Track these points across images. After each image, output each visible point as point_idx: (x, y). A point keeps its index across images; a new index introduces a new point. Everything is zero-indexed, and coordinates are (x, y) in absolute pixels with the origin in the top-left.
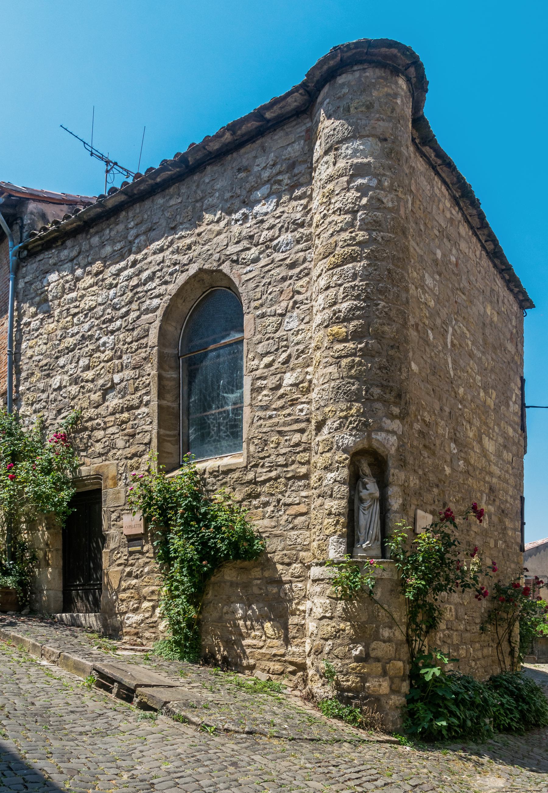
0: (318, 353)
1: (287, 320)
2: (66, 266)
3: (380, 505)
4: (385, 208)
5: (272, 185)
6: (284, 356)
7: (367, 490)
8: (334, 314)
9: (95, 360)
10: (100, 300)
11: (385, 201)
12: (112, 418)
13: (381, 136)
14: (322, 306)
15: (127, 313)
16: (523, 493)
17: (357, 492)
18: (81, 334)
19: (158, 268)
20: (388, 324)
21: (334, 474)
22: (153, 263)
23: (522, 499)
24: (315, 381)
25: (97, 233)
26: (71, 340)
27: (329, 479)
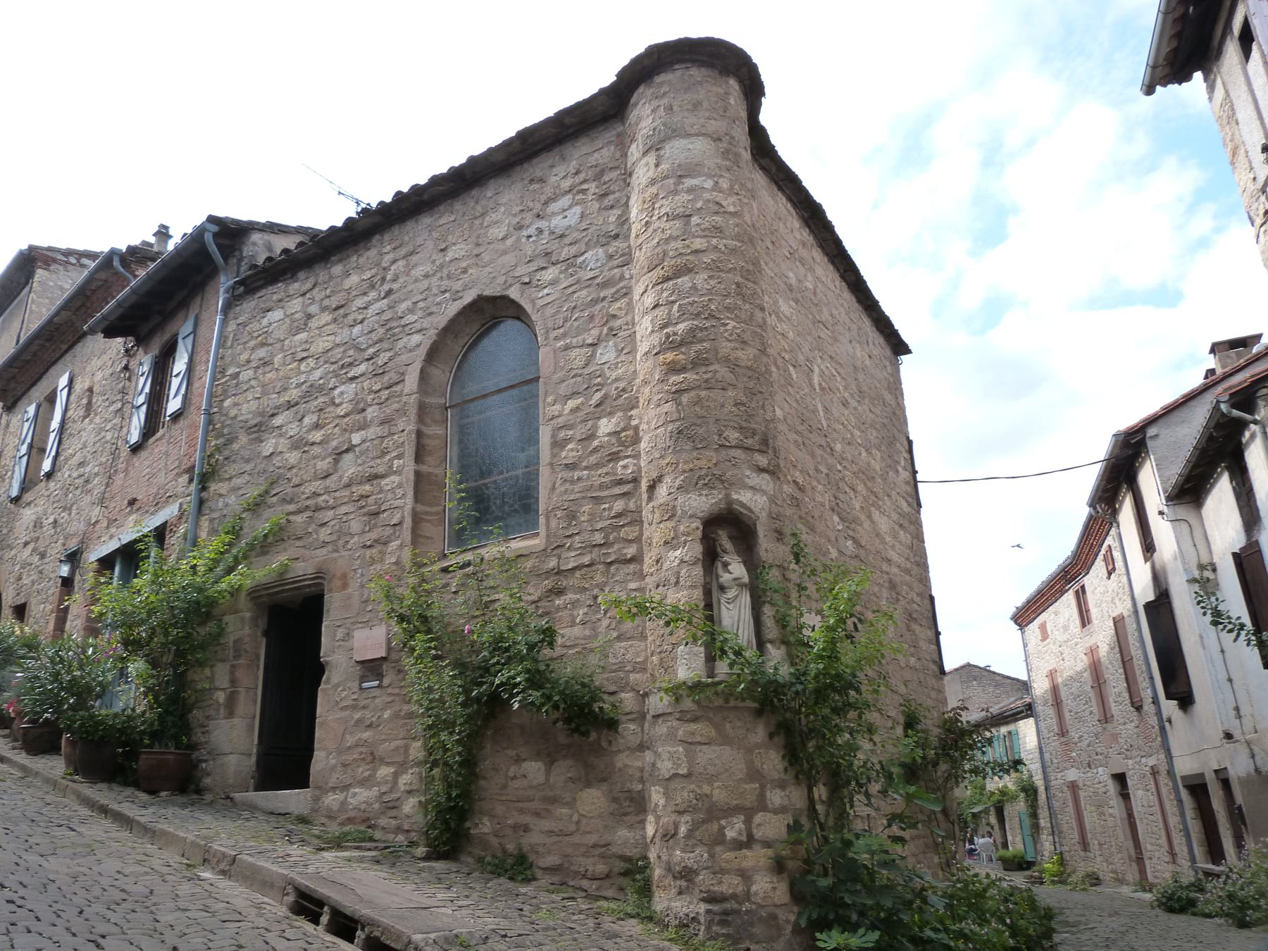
0: (647, 390)
1: (599, 351)
2: (295, 301)
3: (751, 596)
4: (726, 212)
5: (574, 195)
6: (598, 396)
7: (730, 573)
8: (668, 338)
9: (326, 415)
10: (338, 340)
11: (724, 203)
12: (346, 493)
13: (714, 136)
14: (649, 330)
15: (376, 355)
16: (930, 589)
17: (714, 577)
18: (308, 384)
19: (421, 297)
20: (742, 349)
21: (679, 551)
22: (415, 292)
23: (932, 599)
24: (643, 426)
25: (340, 261)
26: (295, 391)
27: (672, 559)
